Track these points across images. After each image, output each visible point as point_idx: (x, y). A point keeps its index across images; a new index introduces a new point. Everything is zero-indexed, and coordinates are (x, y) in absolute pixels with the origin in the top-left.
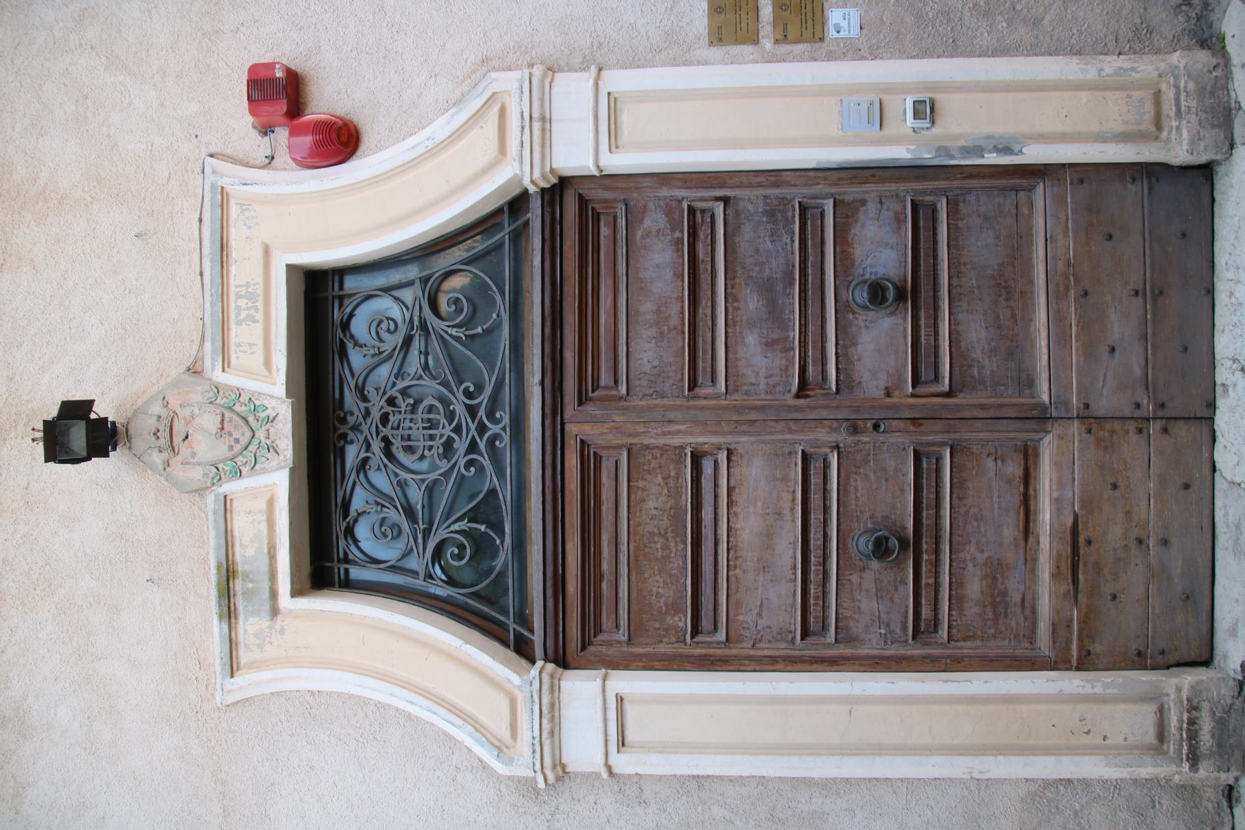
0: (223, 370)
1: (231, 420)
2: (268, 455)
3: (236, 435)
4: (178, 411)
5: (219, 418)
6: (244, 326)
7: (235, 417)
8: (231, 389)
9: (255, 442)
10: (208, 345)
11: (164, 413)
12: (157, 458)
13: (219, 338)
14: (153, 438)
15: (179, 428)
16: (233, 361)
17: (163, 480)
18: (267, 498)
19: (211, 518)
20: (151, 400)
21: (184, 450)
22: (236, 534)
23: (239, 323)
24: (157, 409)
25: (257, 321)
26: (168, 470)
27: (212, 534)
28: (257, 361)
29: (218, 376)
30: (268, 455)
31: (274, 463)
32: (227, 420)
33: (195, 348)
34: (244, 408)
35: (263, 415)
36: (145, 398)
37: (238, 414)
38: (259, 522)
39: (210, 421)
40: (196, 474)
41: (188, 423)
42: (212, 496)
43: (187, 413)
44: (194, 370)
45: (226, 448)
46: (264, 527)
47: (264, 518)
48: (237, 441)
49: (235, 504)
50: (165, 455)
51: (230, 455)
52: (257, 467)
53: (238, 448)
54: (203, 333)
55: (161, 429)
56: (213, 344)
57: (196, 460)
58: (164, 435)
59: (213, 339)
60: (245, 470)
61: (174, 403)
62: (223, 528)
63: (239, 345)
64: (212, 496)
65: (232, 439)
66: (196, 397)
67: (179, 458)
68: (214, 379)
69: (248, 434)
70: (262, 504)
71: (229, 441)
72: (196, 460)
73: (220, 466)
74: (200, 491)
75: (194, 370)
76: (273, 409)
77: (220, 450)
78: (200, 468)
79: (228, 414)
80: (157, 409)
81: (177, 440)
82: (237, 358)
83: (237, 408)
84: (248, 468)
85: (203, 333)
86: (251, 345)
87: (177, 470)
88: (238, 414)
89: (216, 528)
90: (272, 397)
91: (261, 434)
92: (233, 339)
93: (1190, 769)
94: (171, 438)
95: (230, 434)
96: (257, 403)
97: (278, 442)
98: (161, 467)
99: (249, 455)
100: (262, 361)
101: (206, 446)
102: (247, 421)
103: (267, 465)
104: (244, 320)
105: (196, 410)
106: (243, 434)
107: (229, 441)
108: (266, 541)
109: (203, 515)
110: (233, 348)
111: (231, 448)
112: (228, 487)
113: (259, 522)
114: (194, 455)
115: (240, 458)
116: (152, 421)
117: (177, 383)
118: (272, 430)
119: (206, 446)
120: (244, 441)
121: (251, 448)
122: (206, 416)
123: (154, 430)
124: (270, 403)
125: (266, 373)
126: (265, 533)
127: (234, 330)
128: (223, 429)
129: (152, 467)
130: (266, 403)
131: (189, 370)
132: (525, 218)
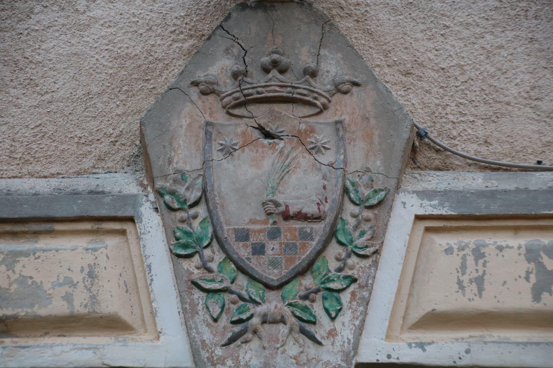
0: (419, 218)
1: (306, 236)
2: (224, 321)
3: (273, 248)
4: (329, 117)
5: (311, 209)
6: (524, 266)
7: (313, 245)
8: (378, 236)
9: (255, 291)
10: (476, 181)
11: (322, 85)
12: (220, 67)
13: (495, 209)
14: (266, 59)
15: (291, 117)
16: (442, 241)
17: (171, 76)
18: (125, 315)
19: (83, 184)
20: (351, 54)
21: (236, 130)
22: (44, 243)
23: (532, 254)
24: (332, 68)
25: (537, 297)
26: (194, 92)
27: (43, 186)
28: (442, 295)
29: (407, 207)
30: (224, 321)
31: (207, 335)
32: (307, 226)
33: (471, 150)
34: (333, 265)
35: (318, 309)
36: (358, 40)
37: (319, 253)
38: (68, 298)
39: (304, 188)
40: (184, 155)
41: (300, 138)
42: (133, 189)
43: (324, 135)
44: (420, 150)
45: (243, 224)
46: (57, 307)
47: (79, 306)
48: (259, 250)
49: (112, 242)
50: (228, 86)
51: (227, 232)
52: (197, 294)
53: (243, 251)
54: (507, 168)
55: (288, 78)
56: (481, 194)
57: (217, 156)
58: (273, 83)
59: (492, 195)
60: (191, 266)
61: (345, 108)
62: (60, 213)
63: (478, 254)
64: (133, 189)
65: (262, 238)
66: (357, 156)
67: (221, 118)
68: (401, 197)
69: (274, 275)
70: (112, 303)
71: (259, 229)
72: (217, 156)
73: (201, 210)
74: (143, 160)
75: (420, 150)
76: (332, 333)
77: (239, 212)
78: (197, 163)
79: (319, 229)
80: (332, 68)
81: (261, 113)
82: (449, 251)
83: (334, 250)
84: (197, 274)
85: (507, 168)
86: (479, 281)
87: (191, 114)
88: (319, 253)
89: (59, 195)
90: (360, 331)
91: (273, 304)
92: (491, 240)
93: (264, 255)
94: (268, 99)
95: (274, 234)
96: (345, 297)
97: (255, 344)
98: (200, 76)
99: (224, 275)
100: (442, 307)
101: (248, 178)
102: (302, 272)
103: (202, 316)
104: (540, 266)
105: (327, 158)
106: (274, 264)
107: (259, 229)
108: (21, 312)
109: (87, 163)
110: (470, 240)
111: (243, 236)
112: (152, 226)
113: (68, 298)
114: (228, 151)
115: (219, 257)
116: (305, 59)
117: (389, 112)
118: (283, 329)
119: (248, 178)
120: (257, 265)
121: (242, 280)
122: (315, 180)
123: (284, 60)
124: (345, 325)
125: (415, 315)
126: (43, 312)
127: (517, 241)
128: (286, 216)
129: (199, 56)
130: (346, 317)
131: (421, 135)
132: (3, 340)
